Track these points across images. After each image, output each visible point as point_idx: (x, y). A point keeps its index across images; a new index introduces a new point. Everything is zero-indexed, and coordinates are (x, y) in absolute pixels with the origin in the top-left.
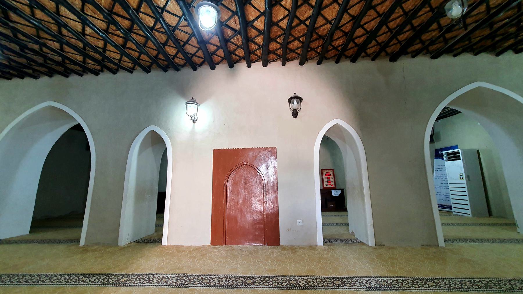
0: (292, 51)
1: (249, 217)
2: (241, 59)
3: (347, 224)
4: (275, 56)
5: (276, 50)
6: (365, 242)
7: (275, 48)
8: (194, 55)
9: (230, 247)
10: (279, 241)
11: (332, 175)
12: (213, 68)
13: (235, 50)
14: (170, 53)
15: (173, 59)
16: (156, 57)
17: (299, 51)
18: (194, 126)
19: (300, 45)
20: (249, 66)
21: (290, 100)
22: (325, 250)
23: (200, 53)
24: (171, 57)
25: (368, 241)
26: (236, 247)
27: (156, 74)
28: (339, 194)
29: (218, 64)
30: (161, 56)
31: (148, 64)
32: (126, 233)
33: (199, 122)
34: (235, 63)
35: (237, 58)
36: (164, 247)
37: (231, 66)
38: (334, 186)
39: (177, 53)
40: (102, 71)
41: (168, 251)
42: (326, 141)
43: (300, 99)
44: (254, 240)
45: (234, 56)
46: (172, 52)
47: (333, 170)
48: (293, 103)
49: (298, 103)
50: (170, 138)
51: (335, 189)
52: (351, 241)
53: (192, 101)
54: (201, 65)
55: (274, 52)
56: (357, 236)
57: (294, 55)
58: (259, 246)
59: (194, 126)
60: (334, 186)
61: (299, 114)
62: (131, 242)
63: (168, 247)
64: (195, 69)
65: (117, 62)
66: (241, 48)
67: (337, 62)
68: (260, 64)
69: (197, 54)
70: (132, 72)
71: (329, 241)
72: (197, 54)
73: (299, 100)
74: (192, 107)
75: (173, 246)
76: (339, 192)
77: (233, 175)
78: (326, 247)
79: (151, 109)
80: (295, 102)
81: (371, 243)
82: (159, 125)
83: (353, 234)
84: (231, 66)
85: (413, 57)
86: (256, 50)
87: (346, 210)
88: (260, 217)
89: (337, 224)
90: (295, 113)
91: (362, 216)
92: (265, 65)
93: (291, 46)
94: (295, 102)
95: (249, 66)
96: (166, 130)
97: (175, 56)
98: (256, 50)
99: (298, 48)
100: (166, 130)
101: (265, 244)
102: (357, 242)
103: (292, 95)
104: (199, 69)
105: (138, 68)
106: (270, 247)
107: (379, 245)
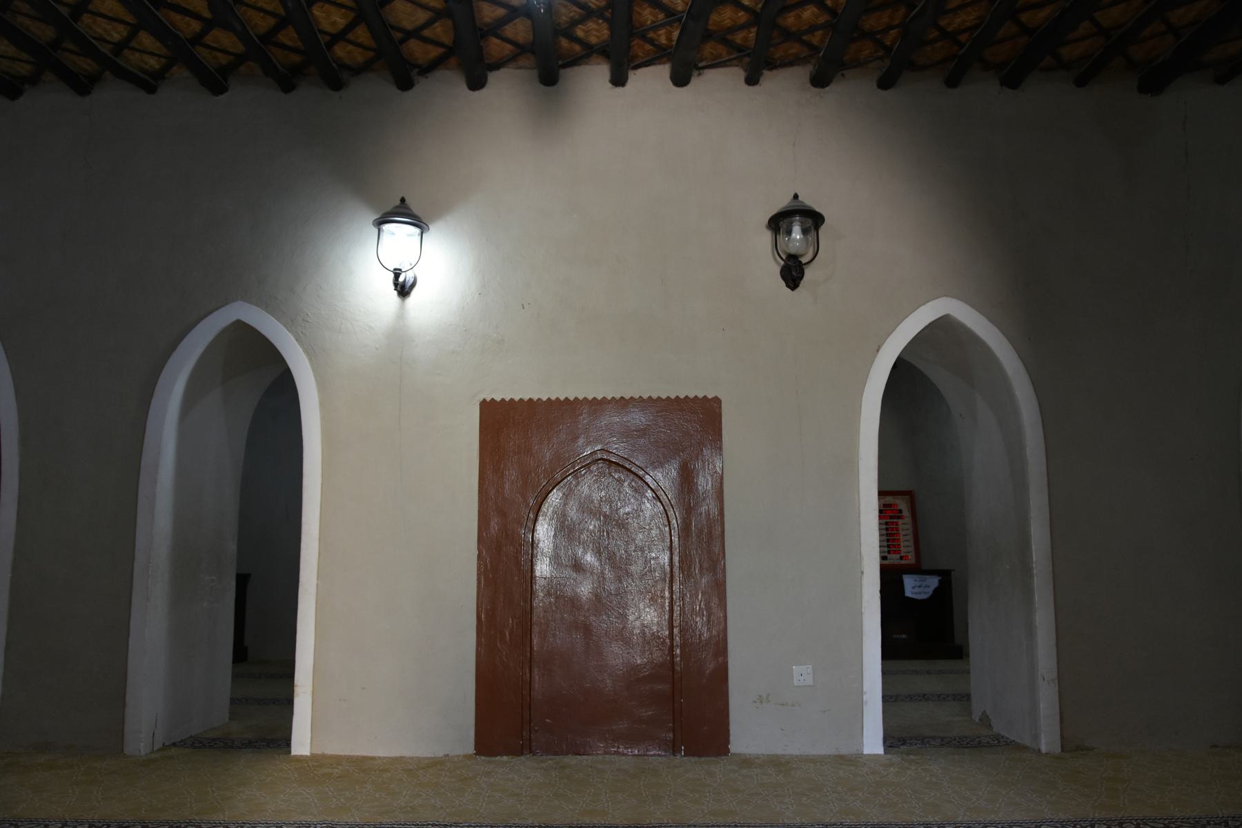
0: (788, 35)
1: (616, 656)
2: (588, 53)
3: (968, 697)
4: (721, 49)
5: (733, 29)
6: (1027, 741)
7: (728, 23)
8: (415, 33)
9: (550, 761)
10: (727, 741)
11: (906, 513)
12: (476, 83)
13: (574, 23)
14: (326, 26)
15: (330, 45)
16: (268, 37)
17: (816, 38)
18: (402, 308)
19: (822, 20)
20: (619, 80)
21: (778, 223)
22: (892, 765)
23: (441, 31)
24: (323, 39)
25: (1036, 737)
26: (571, 760)
27: (249, 100)
28: (930, 590)
29: (496, 66)
30: (289, 37)
31: (223, 59)
32: (148, 709)
33: (406, 290)
34: (565, 66)
35: (577, 48)
36: (300, 759)
37: (549, 78)
38: (911, 559)
39: (350, 27)
40: (34, 80)
41: (330, 770)
42: (906, 384)
43: (813, 219)
44: (632, 738)
45: (564, 43)
46: (334, 24)
47: (909, 494)
48: (789, 233)
49: (805, 232)
50: (310, 352)
51: (916, 570)
52: (982, 743)
53: (400, 211)
54: (428, 69)
55: (723, 37)
56: (999, 727)
57: (795, 49)
58: (656, 757)
59: (402, 308)
60: (911, 559)
61: (809, 273)
62: (165, 747)
63: (316, 761)
64: (405, 84)
65: (105, 49)
66: (601, 16)
67: (952, 82)
68: (662, 72)
69: (426, 33)
70: (151, 90)
71: (903, 741)
72: (426, 33)
73: (809, 222)
74: (399, 235)
75: (338, 760)
76: (933, 582)
77: (555, 497)
78: (896, 759)
79: (238, 244)
80: (797, 234)
81: (1048, 741)
82: (270, 305)
83: (985, 720)
84: (549, 78)
85: (1221, 80)
86: (655, 28)
87: (958, 652)
88: (658, 656)
89: (924, 697)
90: (793, 272)
91: (1021, 654)
92: (680, 80)
93: (790, 20)
94: (797, 234)
95: (619, 80)
96: (292, 322)
97: (340, 36)
98: (655, 28)
99: (812, 29)
100: (292, 322)
101: (675, 751)
102: (1000, 743)
103: (782, 202)
104: (423, 86)
105: (180, 72)
106: (693, 759)
107: (1071, 745)
